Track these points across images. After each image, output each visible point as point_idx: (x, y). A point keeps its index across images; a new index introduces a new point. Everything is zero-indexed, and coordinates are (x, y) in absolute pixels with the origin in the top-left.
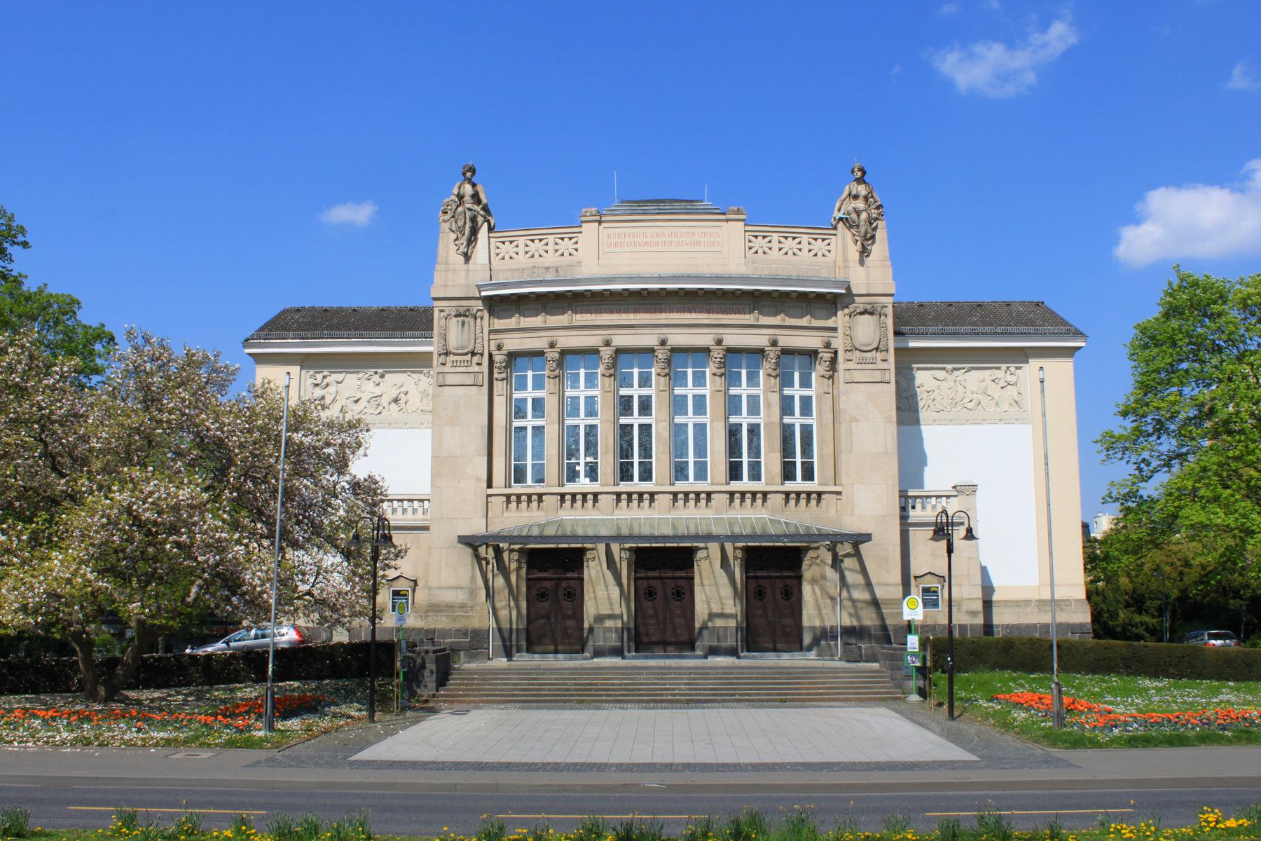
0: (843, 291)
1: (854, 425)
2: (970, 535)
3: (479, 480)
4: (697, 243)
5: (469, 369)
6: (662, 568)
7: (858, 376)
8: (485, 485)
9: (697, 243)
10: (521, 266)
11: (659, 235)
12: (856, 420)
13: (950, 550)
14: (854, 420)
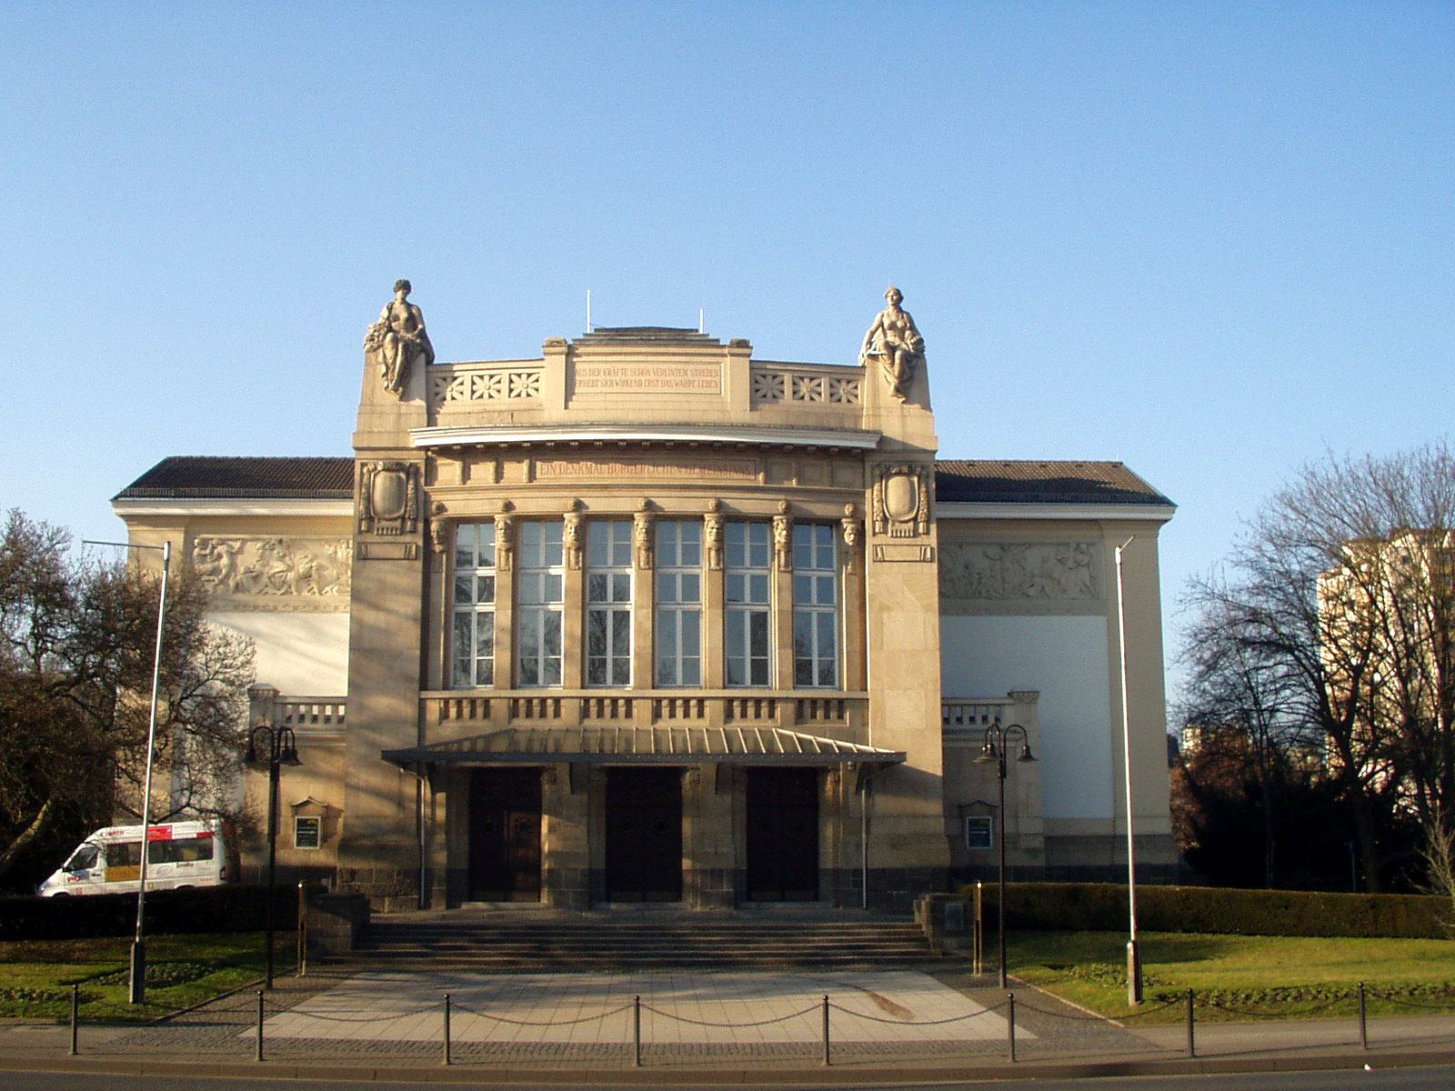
0: (873, 446)
1: (885, 615)
2: (1027, 757)
3: (408, 679)
4: (690, 383)
5: (401, 539)
6: (639, 798)
7: (891, 553)
8: (417, 686)
9: (690, 383)
10: (468, 410)
11: (642, 373)
12: (888, 609)
13: (1003, 775)
14: (884, 608)
